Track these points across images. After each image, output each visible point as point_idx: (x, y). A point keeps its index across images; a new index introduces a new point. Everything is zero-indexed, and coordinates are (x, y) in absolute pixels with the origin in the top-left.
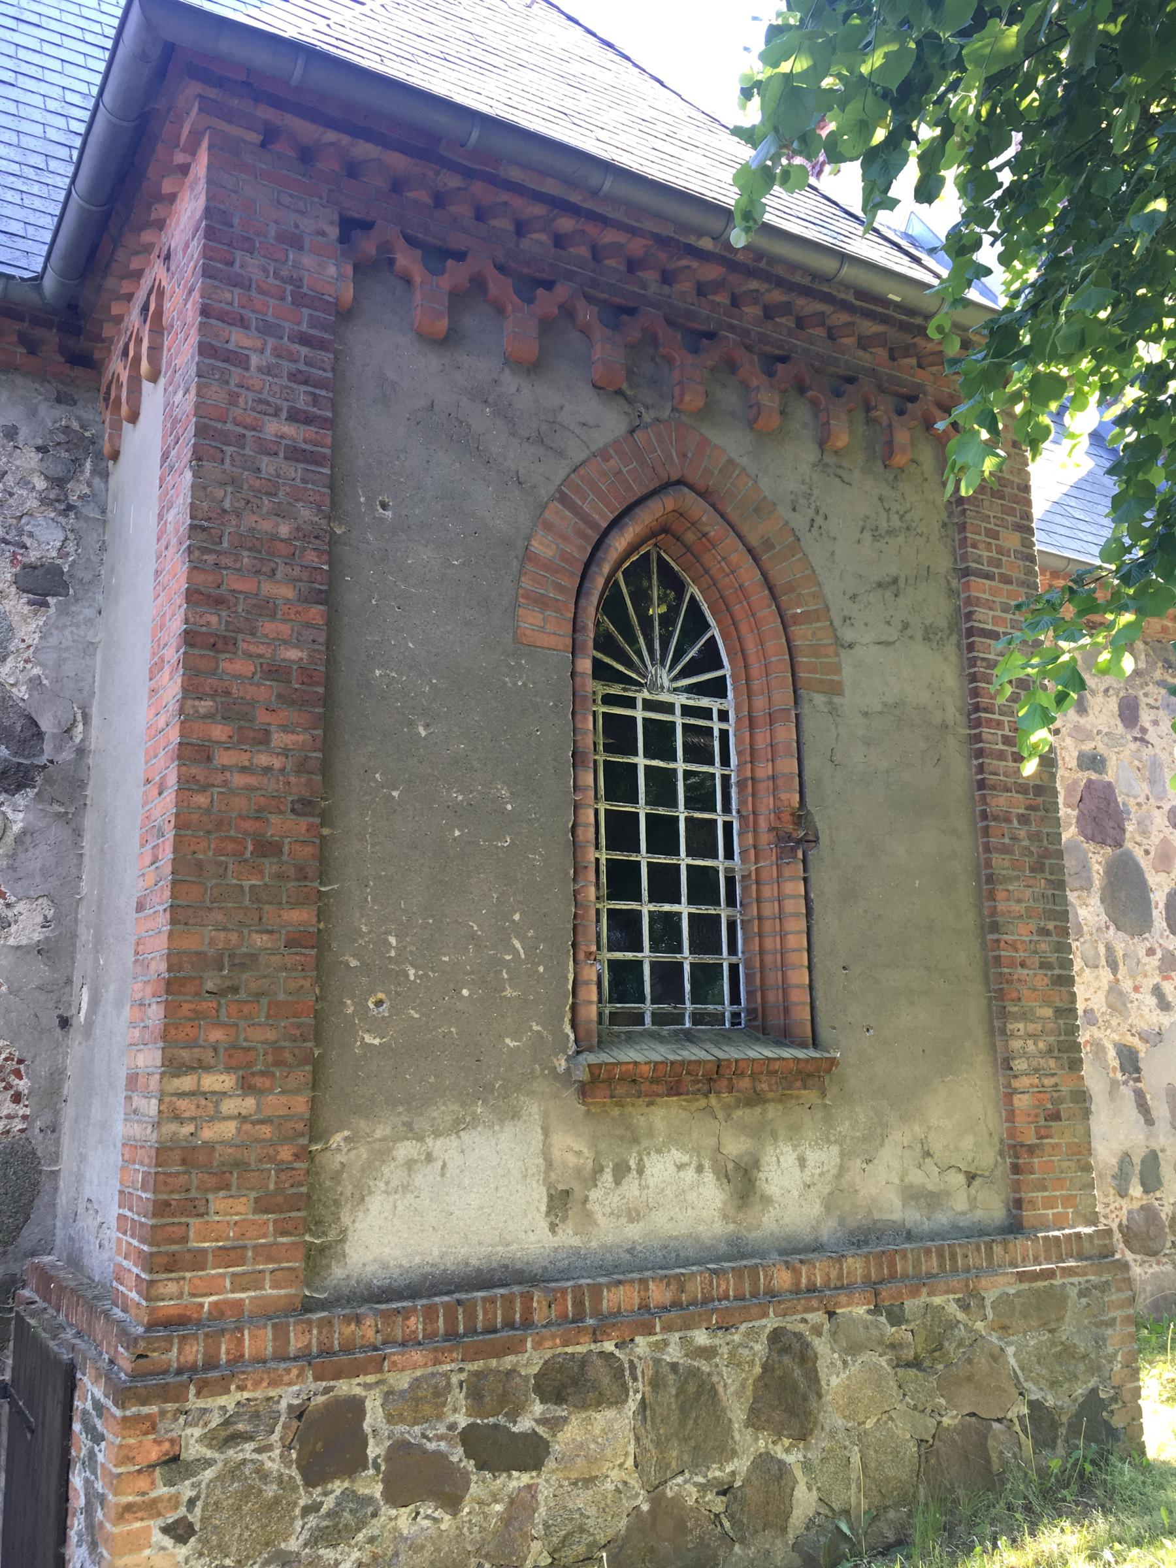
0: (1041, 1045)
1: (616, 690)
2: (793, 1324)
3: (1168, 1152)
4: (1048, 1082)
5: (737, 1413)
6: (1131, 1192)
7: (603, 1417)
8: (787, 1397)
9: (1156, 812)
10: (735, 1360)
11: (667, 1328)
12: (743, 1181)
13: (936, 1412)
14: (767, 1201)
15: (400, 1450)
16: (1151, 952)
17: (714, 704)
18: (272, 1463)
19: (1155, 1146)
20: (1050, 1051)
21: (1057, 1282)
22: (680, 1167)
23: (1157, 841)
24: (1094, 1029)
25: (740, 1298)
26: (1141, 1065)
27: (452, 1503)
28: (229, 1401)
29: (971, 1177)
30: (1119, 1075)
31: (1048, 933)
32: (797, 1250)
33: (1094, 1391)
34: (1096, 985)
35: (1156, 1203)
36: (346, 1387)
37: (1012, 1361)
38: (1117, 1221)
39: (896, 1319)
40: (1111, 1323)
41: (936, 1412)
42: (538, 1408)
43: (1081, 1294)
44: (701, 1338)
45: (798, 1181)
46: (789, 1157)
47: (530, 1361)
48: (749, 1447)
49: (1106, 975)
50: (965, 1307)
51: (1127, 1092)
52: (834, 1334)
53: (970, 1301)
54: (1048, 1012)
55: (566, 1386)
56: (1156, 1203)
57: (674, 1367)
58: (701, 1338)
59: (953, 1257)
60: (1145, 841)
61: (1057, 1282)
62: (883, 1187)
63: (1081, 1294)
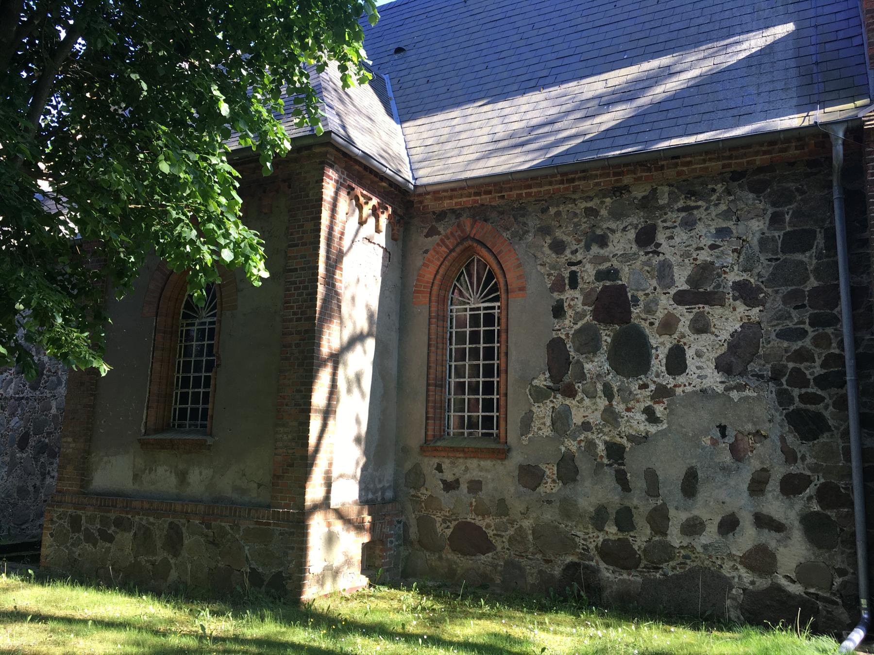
0: (290, 437)
1: (189, 321)
2: (176, 521)
3: (641, 510)
4: (290, 451)
5: (159, 544)
6: (606, 528)
7: (126, 534)
8: (174, 542)
9: (663, 297)
10: (160, 527)
11: (143, 515)
12: (182, 477)
13: (217, 561)
14: (189, 484)
15: (87, 529)
16: (644, 386)
17: (215, 319)
18: (66, 525)
19: (627, 503)
20: (294, 439)
21: (271, 527)
22: (166, 471)
23: (661, 316)
24: (589, 433)
25: (166, 511)
26: (625, 455)
27: (95, 545)
28: (61, 510)
29: (259, 485)
30: (605, 461)
31: (301, 391)
32: (196, 501)
33: (281, 572)
34: (594, 407)
35: (631, 539)
36: (79, 512)
37: (247, 552)
38: (594, 544)
39: (209, 527)
40: (293, 548)
41: (217, 561)
42: (113, 528)
43: (281, 534)
44: (151, 519)
45: (198, 479)
46: (197, 471)
47: (113, 515)
48: (161, 555)
49: (602, 403)
50: (232, 529)
51: (610, 472)
52: (188, 528)
53: (235, 527)
54: (295, 424)
55: (119, 523)
56: (631, 539)
57: (144, 526)
58: (151, 519)
59: (235, 511)
60: (650, 317)
61: (271, 527)
62: (226, 484)
63: (281, 534)
